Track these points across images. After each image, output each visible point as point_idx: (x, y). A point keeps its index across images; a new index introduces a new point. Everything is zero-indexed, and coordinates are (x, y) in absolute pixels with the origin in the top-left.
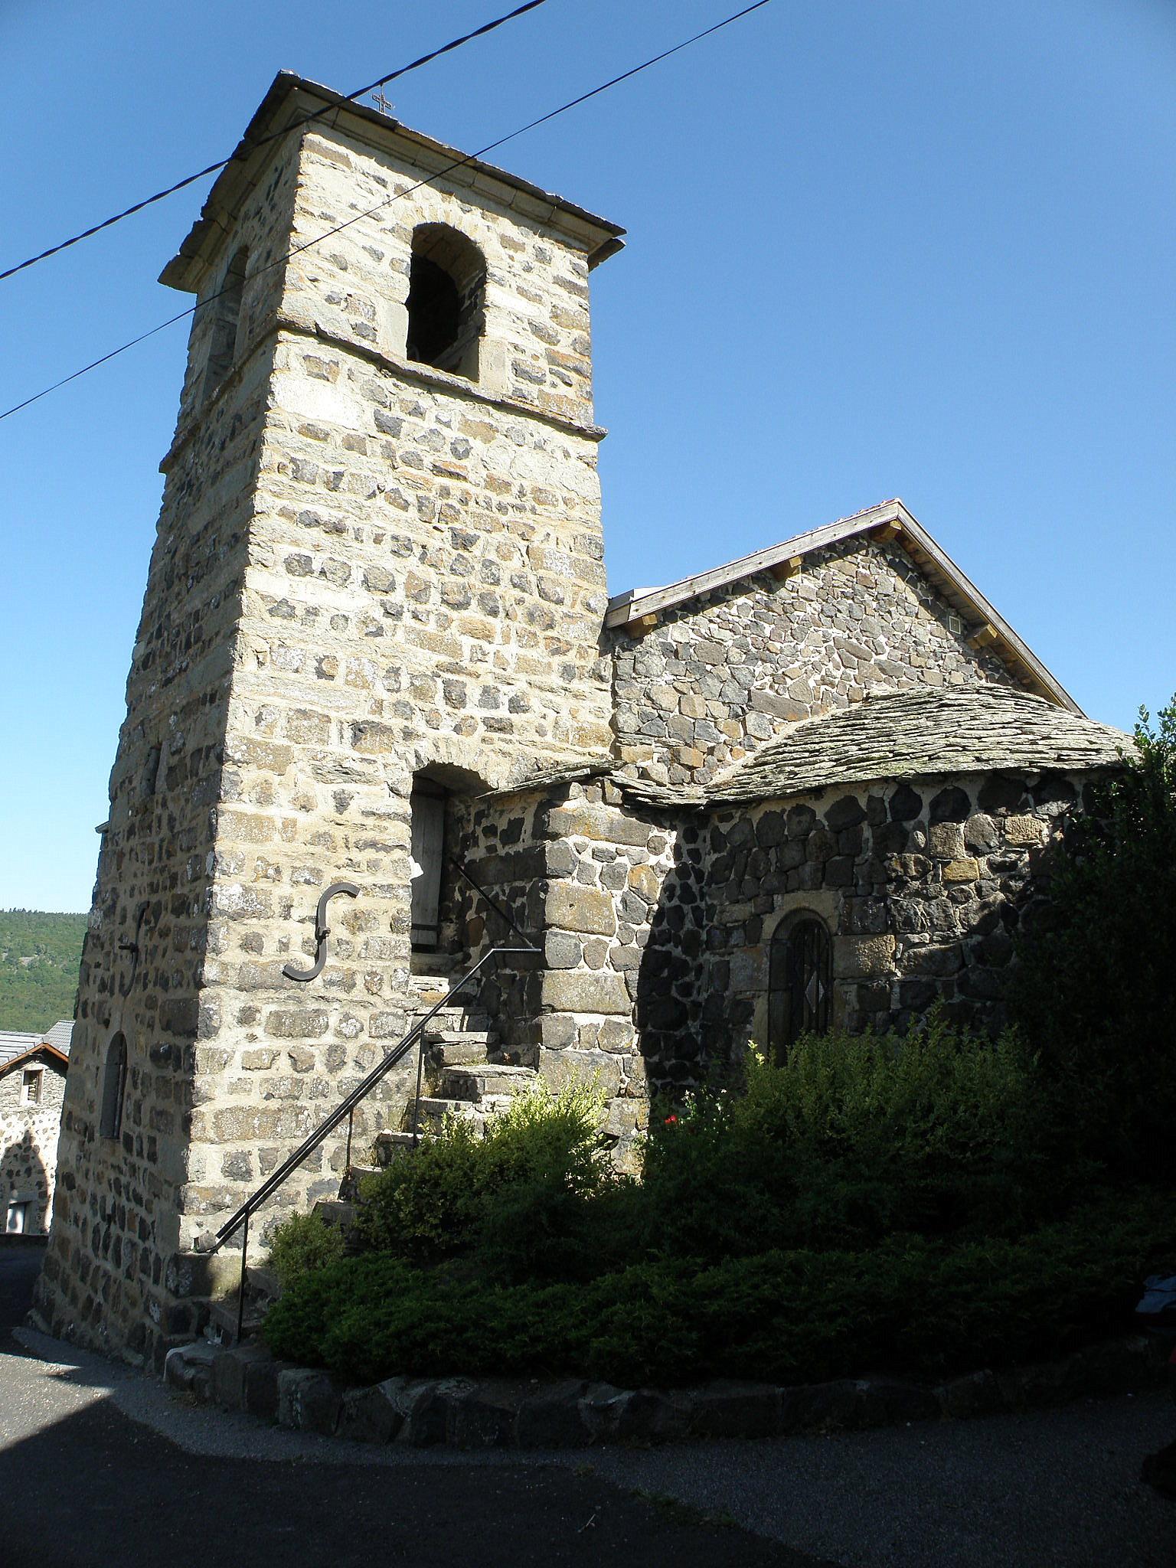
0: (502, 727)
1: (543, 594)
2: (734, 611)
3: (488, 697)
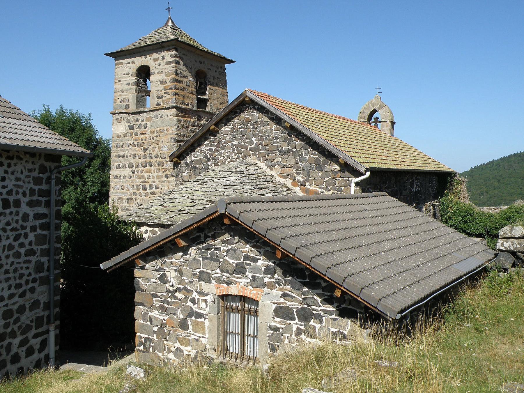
0: (153, 193)
1: (162, 158)
2: (204, 147)
3: (151, 187)
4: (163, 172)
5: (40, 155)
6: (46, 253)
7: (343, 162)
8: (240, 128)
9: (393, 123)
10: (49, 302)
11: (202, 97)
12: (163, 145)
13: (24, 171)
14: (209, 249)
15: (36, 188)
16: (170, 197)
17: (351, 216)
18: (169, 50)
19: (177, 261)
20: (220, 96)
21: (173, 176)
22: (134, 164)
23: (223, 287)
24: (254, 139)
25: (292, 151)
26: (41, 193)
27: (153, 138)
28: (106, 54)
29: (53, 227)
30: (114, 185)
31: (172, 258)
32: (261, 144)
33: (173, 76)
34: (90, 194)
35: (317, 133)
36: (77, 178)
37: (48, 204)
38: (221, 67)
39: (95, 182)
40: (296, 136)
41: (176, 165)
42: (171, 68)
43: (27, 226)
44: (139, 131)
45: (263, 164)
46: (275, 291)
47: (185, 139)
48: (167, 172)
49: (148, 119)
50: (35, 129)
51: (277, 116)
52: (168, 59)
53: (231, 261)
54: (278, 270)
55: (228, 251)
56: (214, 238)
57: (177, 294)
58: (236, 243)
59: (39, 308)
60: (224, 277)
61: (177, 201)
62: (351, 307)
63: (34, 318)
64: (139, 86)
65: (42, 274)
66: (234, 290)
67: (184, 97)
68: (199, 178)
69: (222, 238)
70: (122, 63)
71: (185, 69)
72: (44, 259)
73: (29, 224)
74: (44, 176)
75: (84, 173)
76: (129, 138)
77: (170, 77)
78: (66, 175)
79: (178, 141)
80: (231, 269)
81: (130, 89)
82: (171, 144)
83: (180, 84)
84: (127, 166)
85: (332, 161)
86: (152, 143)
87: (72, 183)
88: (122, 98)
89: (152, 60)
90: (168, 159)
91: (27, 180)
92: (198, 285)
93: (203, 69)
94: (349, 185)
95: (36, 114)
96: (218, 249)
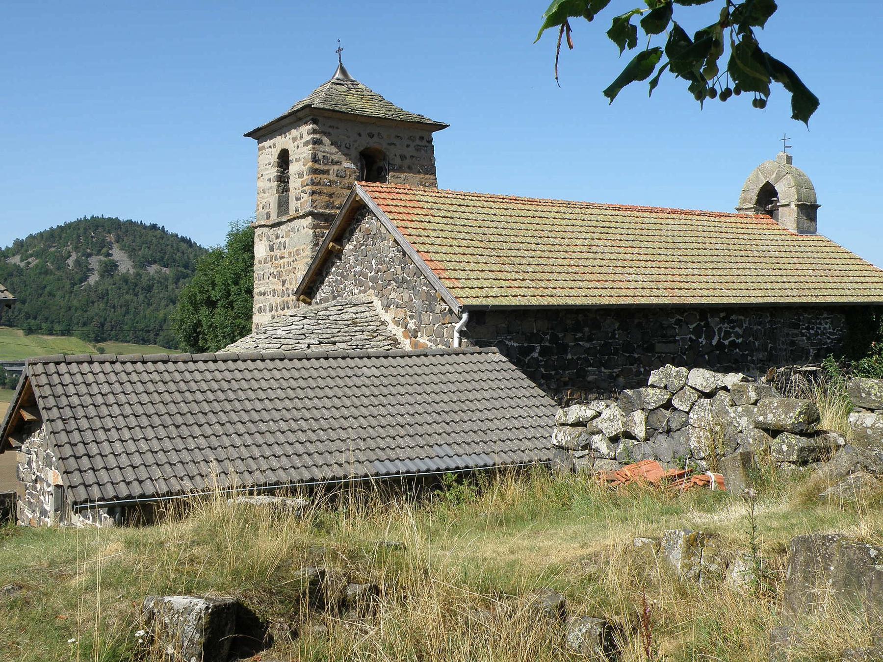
18: (306, 123)
67: (331, 195)
71: (334, 149)
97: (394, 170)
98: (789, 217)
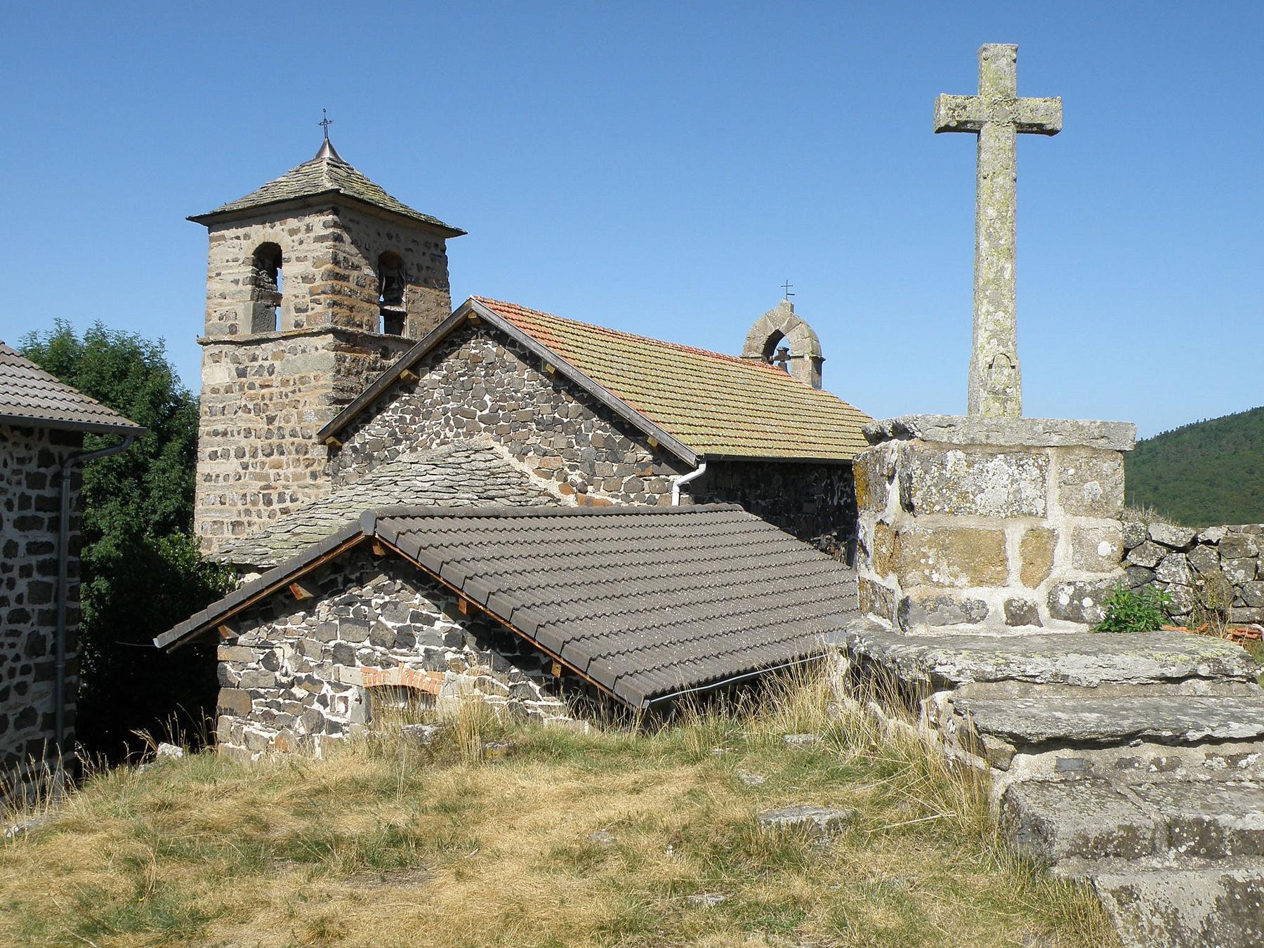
0: (285, 511)
3: (281, 499)
4: (307, 467)
5: (41, 432)
6: (49, 618)
7: (655, 445)
8: (460, 375)
9: (818, 362)
10: (54, 715)
11: (393, 309)
12: (306, 409)
13: (9, 461)
14: (351, 604)
15: (33, 493)
16: (308, 515)
17: (636, 545)
18: (321, 212)
19: (294, 627)
20: (432, 305)
21: (328, 475)
22: (247, 450)
23: (376, 672)
24: (487, 398)
25: (562, 423)
26: (43, 504)
27: (287, 396)
28: (190, 219)
29: (63, 570)
30: (203, 492)
31: (286, 623)
32: (502, 408)
33: (330, 266)
34: (156, 517)
35: (609, 384)
36: (128, 482)
37: (55, 525)
38: (436, 245)
39: (170, 491)
40: (568, 392)
41: (333, 451)
42: (324, 250)
43: (12, 566)
44: (258, 381)
45: (506, 449)
46: (463, 677)
47: (355, 397)
48: (315, 467)
49: (276, 356)
50: (33, 383)
51: (531, 352)
52: (320, 231)
53: (390, 624)
54: (470, 638)
55: (383, 606)
56: (361, 583)
57: (295, 690)
58: (398, 591)
59: (34, 724)
60: (378, 654)
61: (321, 522)
62: (577, 688)
63: (24, 743)
64: (259, 286)
65: (41, 659)
66: (394, 677)
67: (351, 309)
68: (369, 477)
69: (374, 582)
70: (223, 238)
71: (354, 250)
72: (46, 631)
73: (17, 562)
74: (49, 472)
75: (146, 469)
76: (236, 394)
77: (322, 269)
78: (105, 475)
79: (337, 401)
80: (389, 641)
81: (240, 292)
82: (325, 407)
83: (345, 283)
84: (232, 453)
85: (636, 441)
86: (284, 406)
87: (117, 492)
88: (223, 310)
89: (286, 233)
90: (315, 440)
91: (15, 478)
92: (332, 670)
93: (395, 250)
94: (669, 490)
95: (39, 340)
96: (367, 603)
97: (412, 283)
98: (801, 370)
